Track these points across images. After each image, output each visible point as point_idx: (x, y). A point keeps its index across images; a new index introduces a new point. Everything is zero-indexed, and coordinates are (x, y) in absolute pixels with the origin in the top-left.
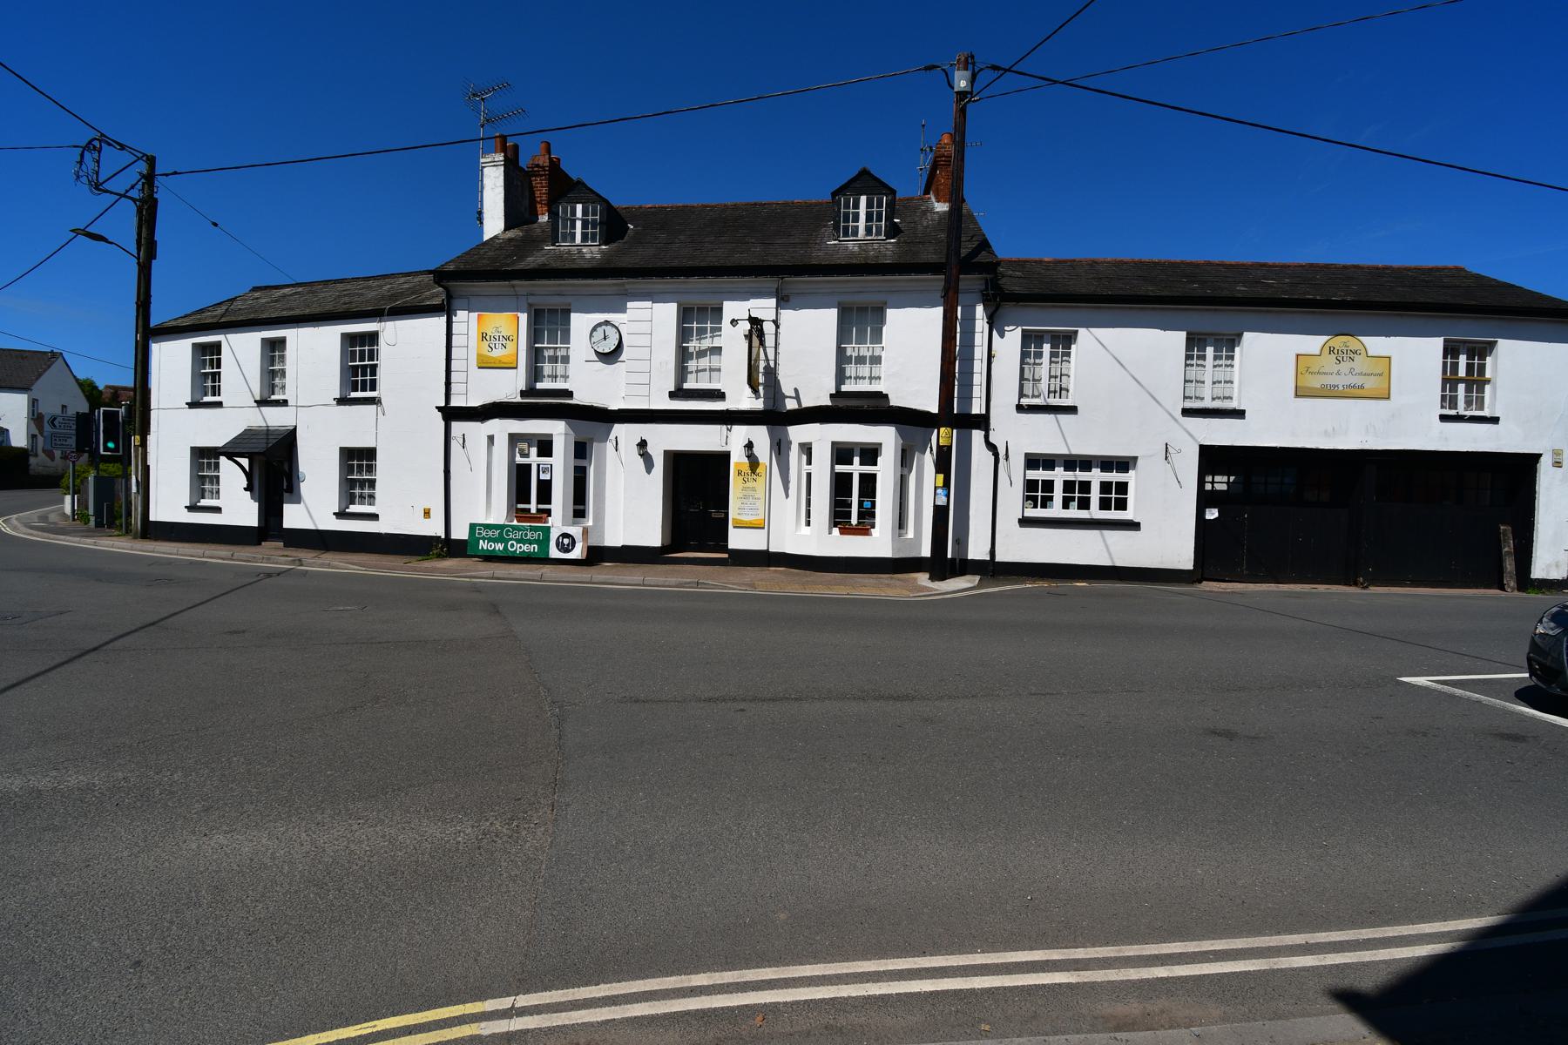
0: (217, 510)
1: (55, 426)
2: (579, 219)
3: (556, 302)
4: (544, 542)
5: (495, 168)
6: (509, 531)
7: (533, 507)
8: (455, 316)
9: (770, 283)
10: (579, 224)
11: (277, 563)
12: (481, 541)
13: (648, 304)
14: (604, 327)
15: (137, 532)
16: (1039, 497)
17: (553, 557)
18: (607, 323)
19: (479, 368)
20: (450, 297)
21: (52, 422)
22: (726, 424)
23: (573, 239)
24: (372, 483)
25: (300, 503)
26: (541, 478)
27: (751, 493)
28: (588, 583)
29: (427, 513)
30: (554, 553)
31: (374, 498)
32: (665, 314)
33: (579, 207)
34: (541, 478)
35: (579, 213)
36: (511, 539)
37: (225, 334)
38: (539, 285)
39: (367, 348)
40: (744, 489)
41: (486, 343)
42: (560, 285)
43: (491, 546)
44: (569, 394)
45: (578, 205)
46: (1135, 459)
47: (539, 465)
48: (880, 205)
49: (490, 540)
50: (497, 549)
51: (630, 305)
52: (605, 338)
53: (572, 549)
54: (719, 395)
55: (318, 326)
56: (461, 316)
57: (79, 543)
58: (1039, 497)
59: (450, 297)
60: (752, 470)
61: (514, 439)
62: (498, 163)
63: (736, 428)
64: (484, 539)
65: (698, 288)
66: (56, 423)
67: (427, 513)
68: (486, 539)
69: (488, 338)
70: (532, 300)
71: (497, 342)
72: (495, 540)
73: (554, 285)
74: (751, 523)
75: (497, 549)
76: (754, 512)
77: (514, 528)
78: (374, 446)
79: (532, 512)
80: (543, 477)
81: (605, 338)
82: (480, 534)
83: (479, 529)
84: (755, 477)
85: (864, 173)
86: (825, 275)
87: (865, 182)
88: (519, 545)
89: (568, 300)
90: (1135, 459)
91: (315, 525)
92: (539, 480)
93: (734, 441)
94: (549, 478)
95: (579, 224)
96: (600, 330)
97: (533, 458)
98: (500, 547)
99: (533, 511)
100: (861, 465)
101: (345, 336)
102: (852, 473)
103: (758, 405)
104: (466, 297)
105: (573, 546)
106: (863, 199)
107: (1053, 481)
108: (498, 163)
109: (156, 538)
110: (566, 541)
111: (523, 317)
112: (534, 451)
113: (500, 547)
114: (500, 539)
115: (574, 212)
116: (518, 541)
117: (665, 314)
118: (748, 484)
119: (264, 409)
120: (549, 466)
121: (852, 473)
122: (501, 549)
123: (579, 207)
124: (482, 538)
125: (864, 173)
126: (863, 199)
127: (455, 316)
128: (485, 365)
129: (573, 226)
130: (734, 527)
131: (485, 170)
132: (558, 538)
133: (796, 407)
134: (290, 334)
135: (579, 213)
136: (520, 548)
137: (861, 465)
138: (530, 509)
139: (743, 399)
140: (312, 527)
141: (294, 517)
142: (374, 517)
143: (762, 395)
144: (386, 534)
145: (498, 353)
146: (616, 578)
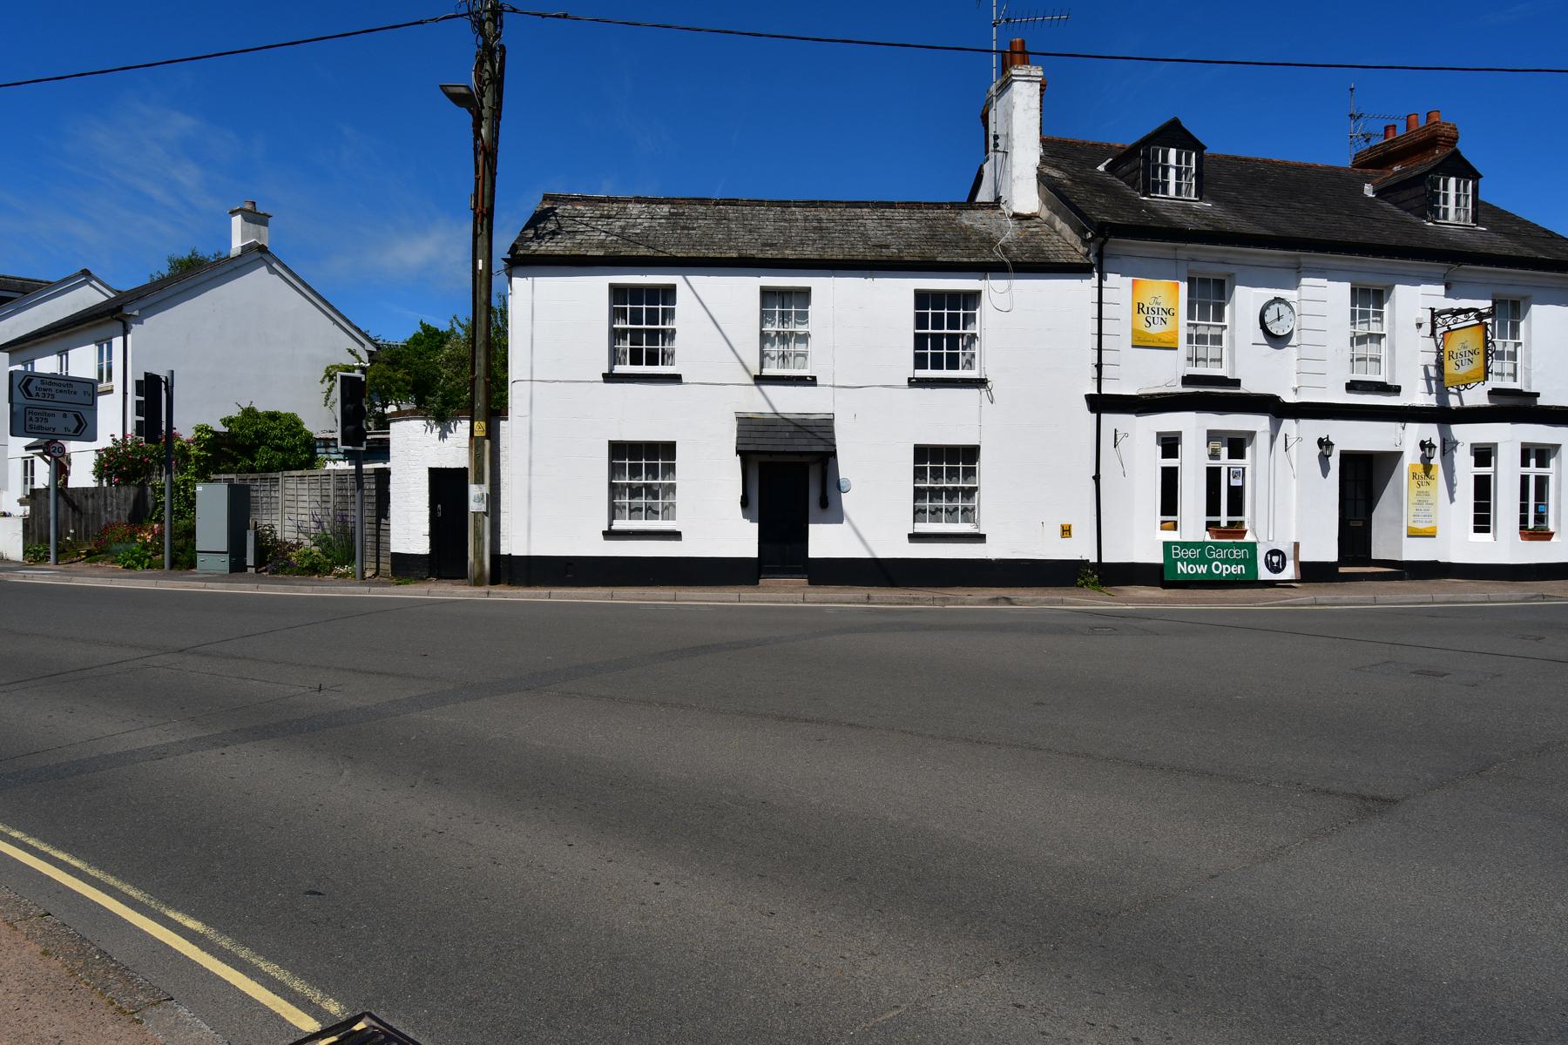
0: (675, 535)
1: (29, 394)
2: (1173, 167)
3: (1216, 271)
4: (1251, 562)
5: (1028, 84)
6: (1210, 549)
7: (1224, 519)
8: (1106, 280)
9: (1438, 268)
10: (1172, 173)
11: (964, 604)
12: (1179, 564)
13: (1323, 282)
14: (1277, 305)
15: (482, 573)
16: (961, 469)
17: (1262, 579)
18: (1278, 300)
19: (1133, 346)
20: (1100, 256)
21: (26, 387)
22: (1401, 422)
23: (1165, 191)
24: (671, 488)
25: (840, 521)
26: (1232, 484)
27: (1425, 498)
28: (1429, 603)
29: (1066, 531)
30: (1264, 574)
31: (675, 507)
32: (1337, 294)
33: (1173, 152)
34: (1232, 484)
35: (1172, 159)
36: (1216, 560)
37: (684, 275)
38: (1207, 250)
39: (946, 311)
40: (1419, 494)
41: (1142, 316)
42: (1228, 252)
43: (1192, 569)
44: (1237, 383)
45: (1171, 149)
46: (1557, 447)
47: (1229, 469)
48: (1188, 161)
49: (1189, 561)
50: (1200, 572)
51: (1304, 281)
52: (1279, 319)
53: (1283, 568)
54: (1396, 390)
55: (873, 277)
56: (1112, 279)
57: (204, 588)
58: (961, 469)
59: (1100, 256)
60: (1425, 472)
61: (1212, 436)
62: (1034, 79)
63: (1409, 425)
64: (1182, 560)
65: (1372, 268)
66: (31, 387)
67: (1066, 531)
68: (1185, 560)
69: (1145, 310)
70: (1193, 266)
71: (1156, 316)
72: (1195, 562)
73: (1221, 251)
74: (1425, 531)
75: (1200, 572)
76: (1428, 519)
77: (1217, 545)
78: (977, 443)
79: (1222, 525)
80: (1234, 483)
81: (1279, 319)
82: (1176, 554)
83: (1176, 549)
84: (1428, 480)
85: (1175, 125)
86: (1534, 269)
87: (1174, 134)
88: (1224, 566)
89: (1232, 269)
90: (1557, 447)
91: (871, 552)
92: (1230, 487)
93: (1407, 439)
94: (1241, 484)
95: (1172, 173)
96: (1274, 308)
97: (1224, 461)
98: (1202, 569)
99: (1224, 524)
100: (1537, 467)
101: (922, 298)
102: (1177, 457)
103: (1431, 401)
104: (1117, 257)
105: (1284, 565)
106: (1452, 181)
107: (1229, 458)
108: (1034, 79)
109: (513, 582)
110: (1275, 559)
111: (1184, 286)
112: (1224, 451)
113: (1202, 569)
114: (1202, 560)
115: (1165, 158)
116: (1224, 562)
117: (1337, 294)
118: (1423, 489)
119: (765, 388)
120: (1241, 470)
121: (1528, 476)
122: (1204, 572)
123: (1173, 152)
124: (1178, 560)
125: (1175, 125)
126: (1452, 181)
127: (1106, 280)
128: (1141, 343)
129: (1165, 174)
130: (1409, 536)
131: (1015, 84)
132: (1266, 557)
133: (1459, 405)
134: (823, 287)
135: (1172, 159)
136: (1227, 569)
137: (1537, 467)
138: (1219, 523)
139: (1417, 395)
140: (868, 556)
141: (824, 541)
142: (675, 535)
143: (1434, 391)
144: (996, 560)
145: (1156, 329)
146: (1460, 596)
